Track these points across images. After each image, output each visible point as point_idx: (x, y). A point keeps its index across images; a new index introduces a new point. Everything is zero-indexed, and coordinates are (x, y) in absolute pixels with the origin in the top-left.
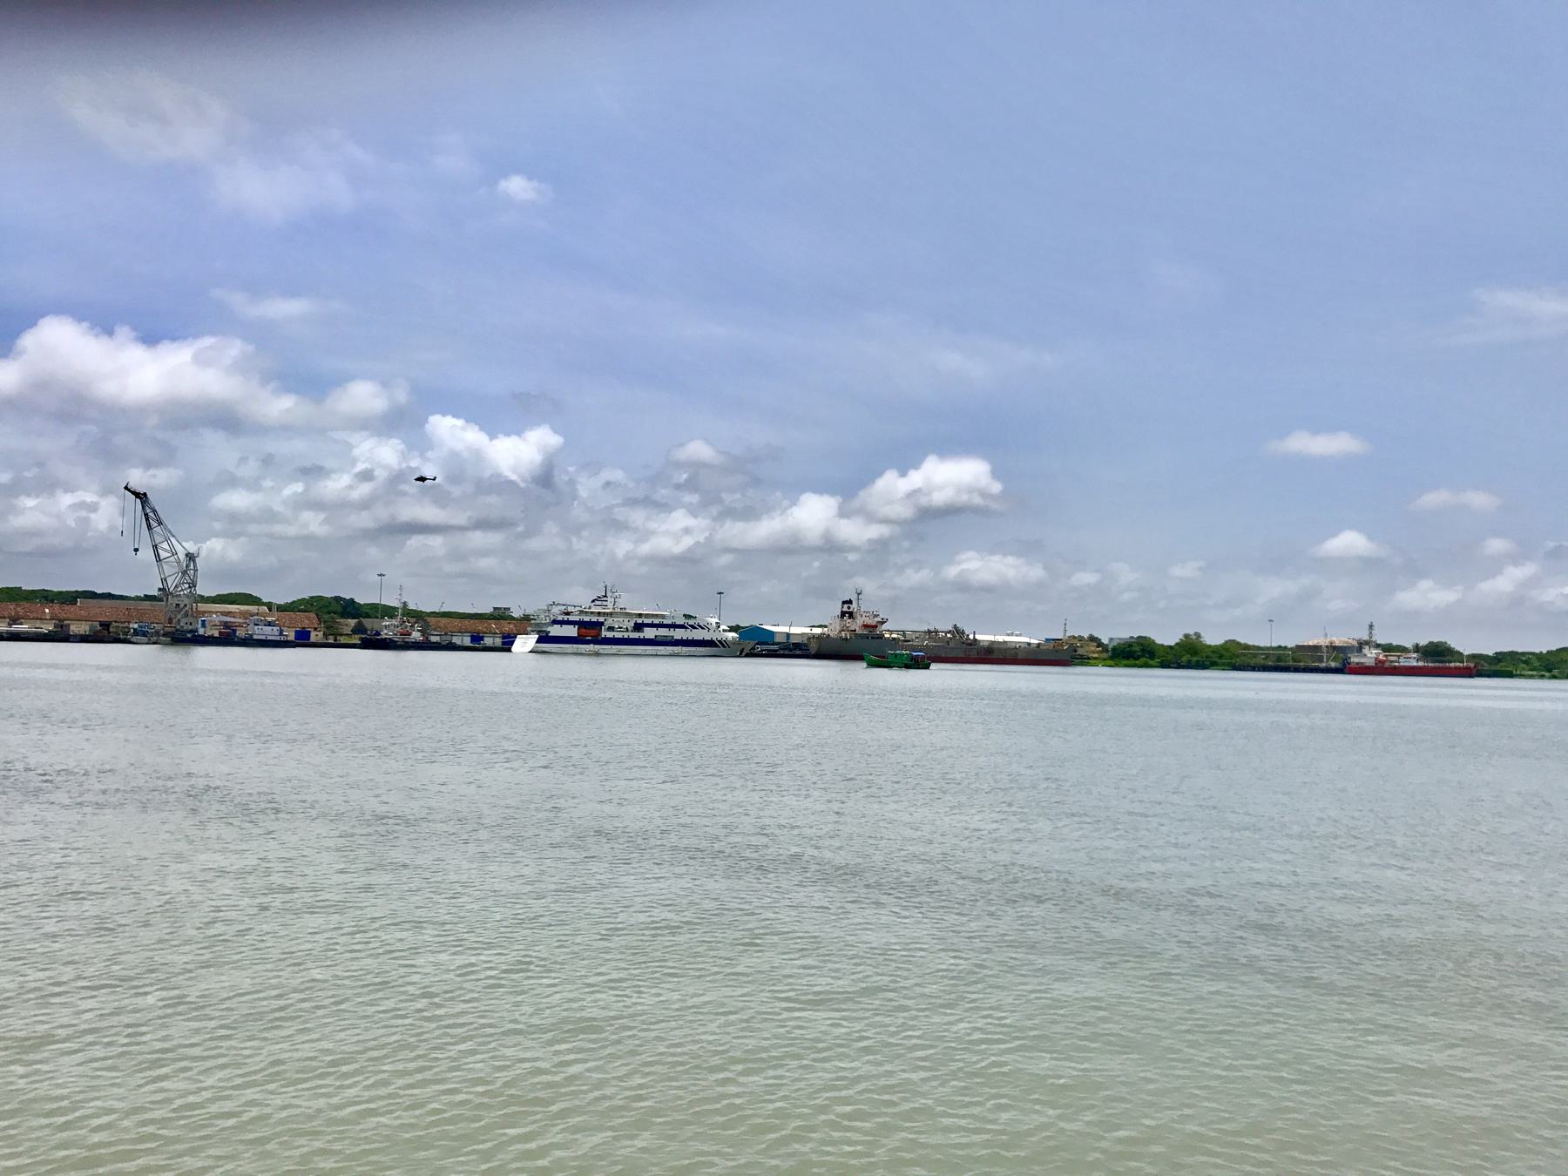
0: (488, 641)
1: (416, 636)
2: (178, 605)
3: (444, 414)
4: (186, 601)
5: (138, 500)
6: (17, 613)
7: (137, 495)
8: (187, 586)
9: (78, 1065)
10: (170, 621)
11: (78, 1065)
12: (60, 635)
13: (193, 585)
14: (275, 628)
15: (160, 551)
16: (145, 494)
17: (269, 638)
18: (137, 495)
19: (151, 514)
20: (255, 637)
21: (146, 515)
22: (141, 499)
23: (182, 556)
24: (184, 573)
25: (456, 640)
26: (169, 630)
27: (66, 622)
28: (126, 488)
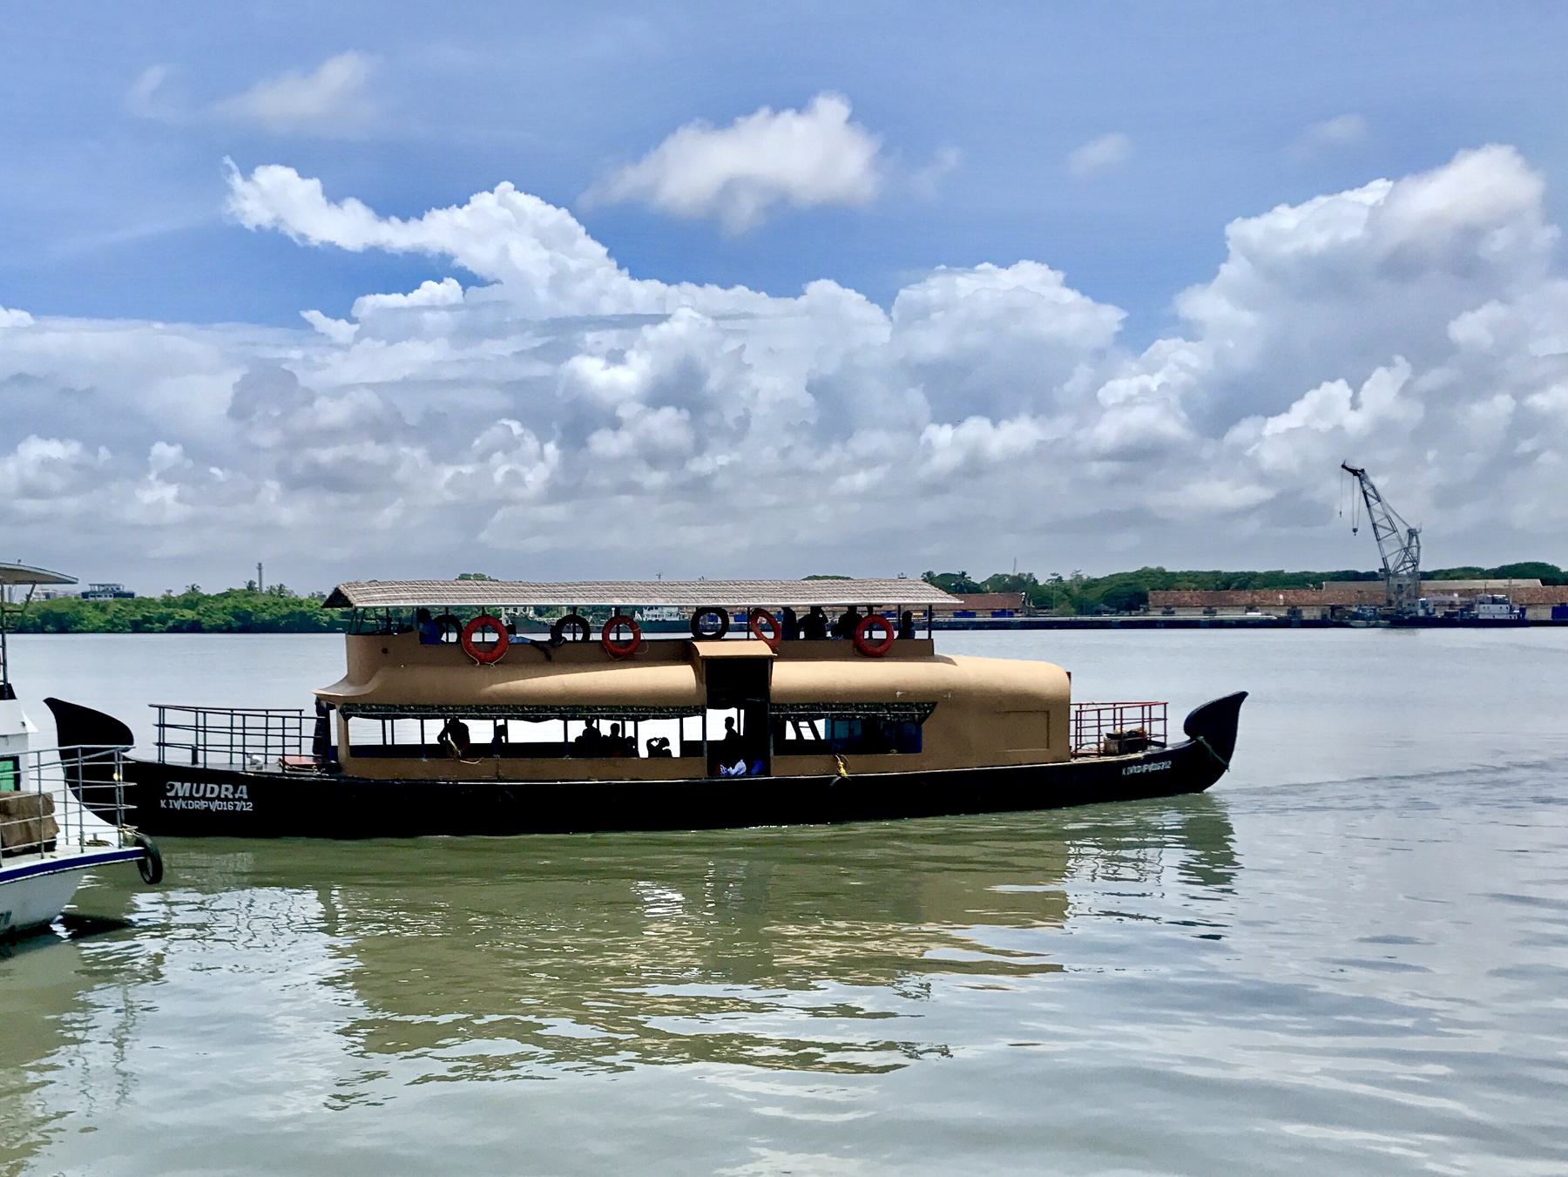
0: (1307, 615)
1: (109, 628)
2: (1400, 586)
3: (364, 295)
4: (1408, 581)
5: (1356, 478)
6: (1254, 601)
7: (1355, 472)
8: (1411, 564)
9: (1039, 1044)
10: (1390, 602)
11: (1039, 1044)
12: (1292, 621)
13: (1415, 562)
14: (1504, 606)
15: (1389, 526)
16: (1363, 471)
17: (1497, 617)
18: (1355, 472)
19: (1370, 491)
20: (1480, 617)
21: (1365, 493)
22: (1359, 475)
23: (1403, 531)
24: (1406, 550)
25: (1530, 614)
26: (1388, 612)
27: (1298, 608)
28: (1344, 466)
